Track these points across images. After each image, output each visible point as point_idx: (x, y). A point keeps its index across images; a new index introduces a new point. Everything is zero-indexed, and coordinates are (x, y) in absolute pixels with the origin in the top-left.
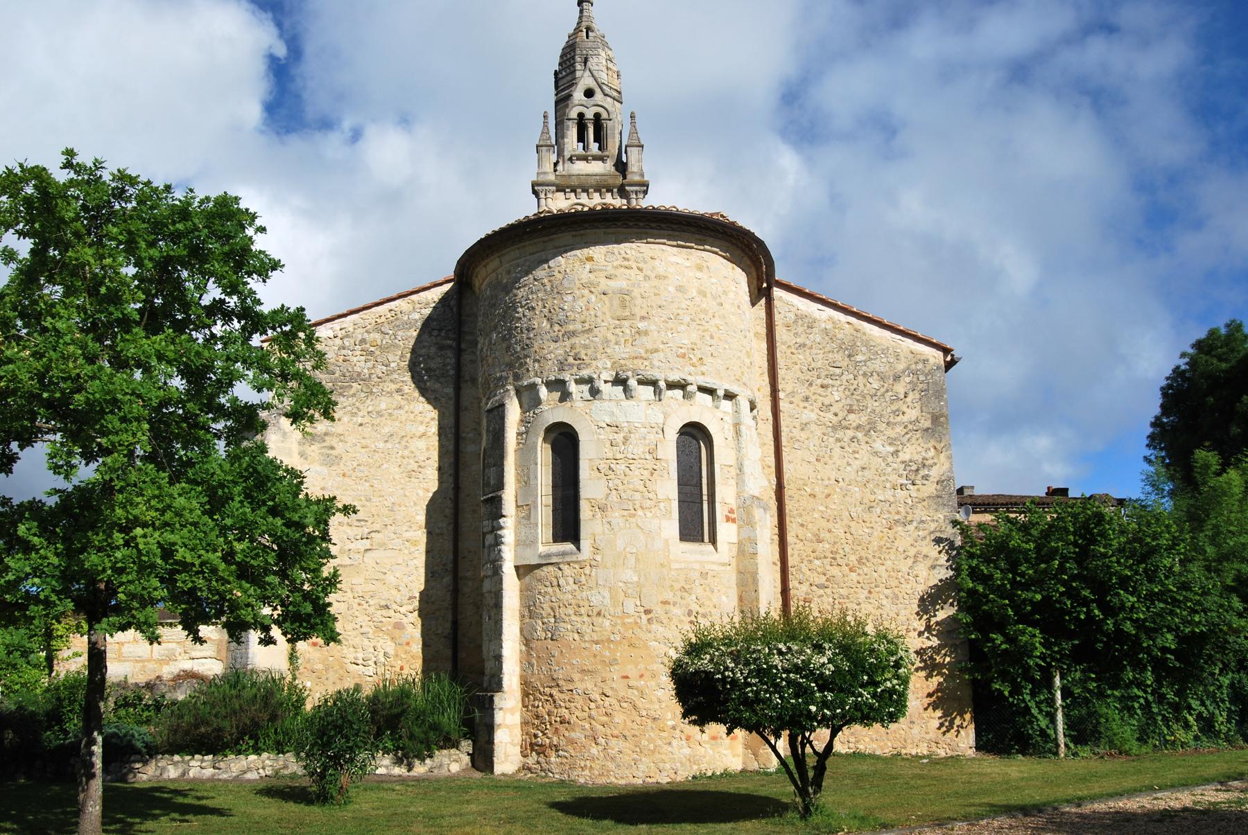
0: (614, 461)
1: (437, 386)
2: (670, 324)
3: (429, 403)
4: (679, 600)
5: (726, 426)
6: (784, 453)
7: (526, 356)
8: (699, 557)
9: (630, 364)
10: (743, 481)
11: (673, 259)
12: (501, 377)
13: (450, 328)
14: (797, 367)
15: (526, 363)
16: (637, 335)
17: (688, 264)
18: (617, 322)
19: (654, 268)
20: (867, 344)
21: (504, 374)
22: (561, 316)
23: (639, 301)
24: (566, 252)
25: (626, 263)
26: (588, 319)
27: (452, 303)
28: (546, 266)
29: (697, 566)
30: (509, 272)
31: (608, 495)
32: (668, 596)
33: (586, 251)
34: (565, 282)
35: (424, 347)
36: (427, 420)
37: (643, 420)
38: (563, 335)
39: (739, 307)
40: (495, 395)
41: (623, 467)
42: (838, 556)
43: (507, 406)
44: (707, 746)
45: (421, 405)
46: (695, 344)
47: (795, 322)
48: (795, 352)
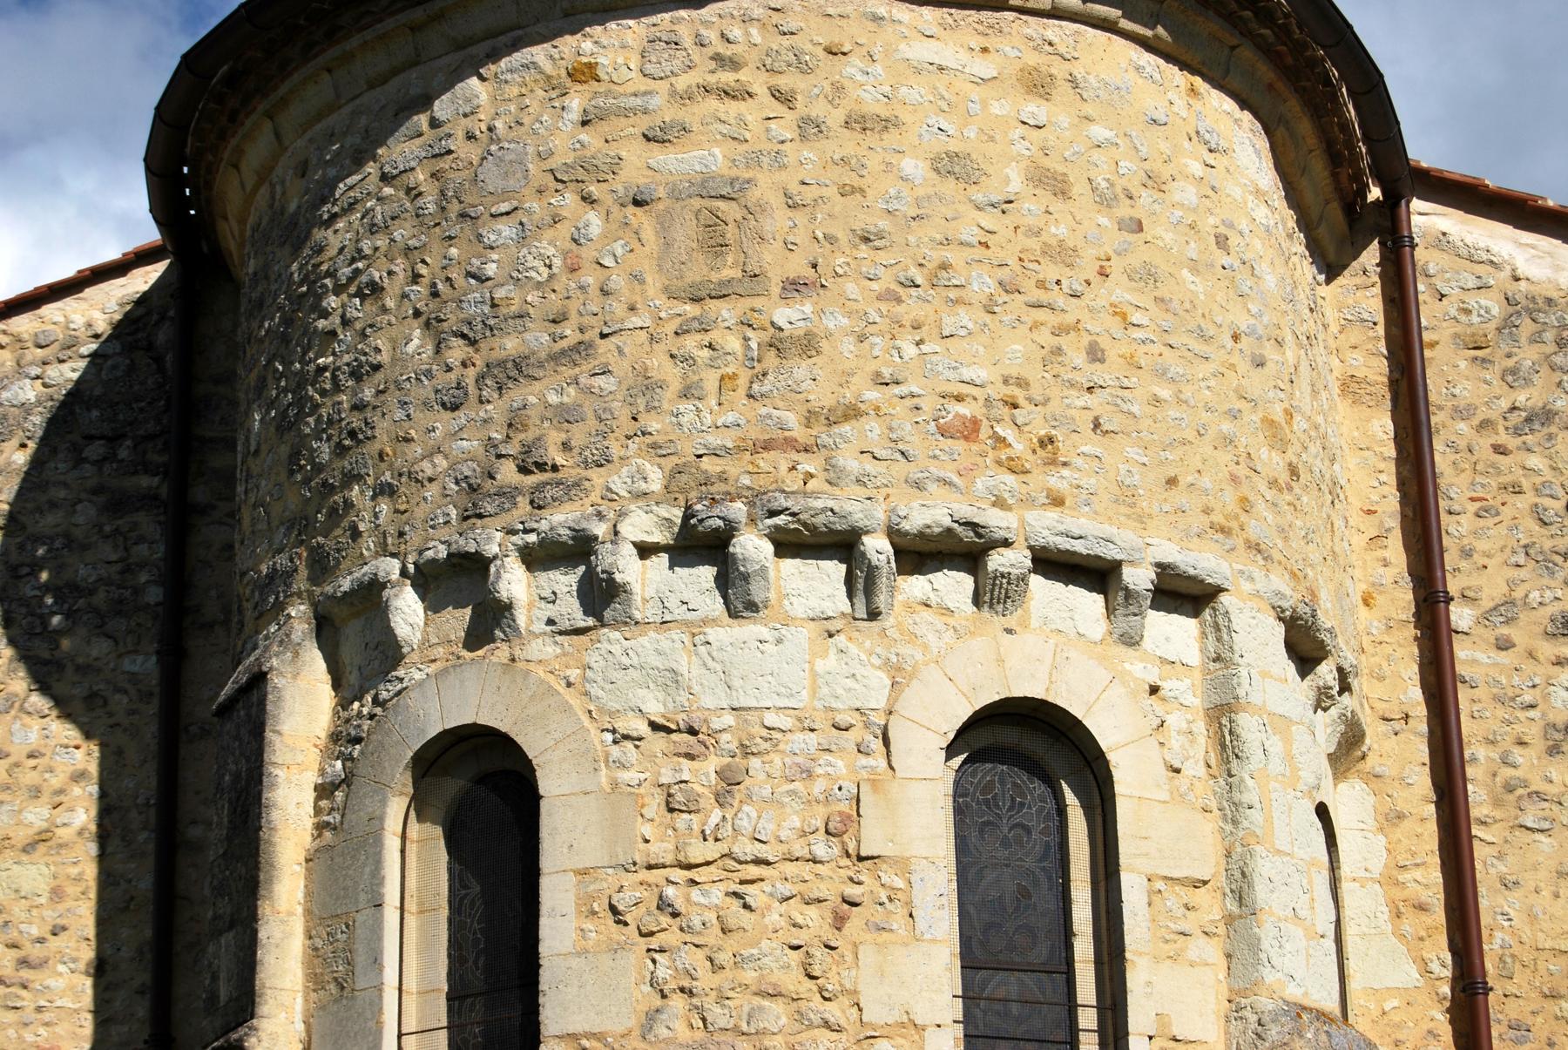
0: (679, 875)
1: (100, 649)
2: (911, 308)
3: (67, 714)
5: (1175, 720)
6: (1480, 851)
7: (351, 478)
9: (739, 472)
10: (1255, 946)
11: (922, 51)
12: (273, 575)
13: (151, 427)
14: (1523, 503)
15: (348, 505)
16: (771, 359)
17: (984, 67)
18: (690, 309)
19: (838, 88)
21: (282, 561)
22: (474, 303)
23: (778, 221)
24: (494, 56)
25: (727, 78)
26: (574, 306)
27: (163, 336)
28: (422, 120)
30: (303, 170)
31: (652, 1016)
33: (568, 43)
34: (491, 176)
35: (53, 505)
36: (55, 782)
37: (803, 700)
38: (480, 379)
39: (1222, 242)
40: (255, 648)
41: (717, 895)
43: (276, 680)
45: (36, 724)
46: (1022, 383)
47: (1507, 326)
48: (1512, 442)
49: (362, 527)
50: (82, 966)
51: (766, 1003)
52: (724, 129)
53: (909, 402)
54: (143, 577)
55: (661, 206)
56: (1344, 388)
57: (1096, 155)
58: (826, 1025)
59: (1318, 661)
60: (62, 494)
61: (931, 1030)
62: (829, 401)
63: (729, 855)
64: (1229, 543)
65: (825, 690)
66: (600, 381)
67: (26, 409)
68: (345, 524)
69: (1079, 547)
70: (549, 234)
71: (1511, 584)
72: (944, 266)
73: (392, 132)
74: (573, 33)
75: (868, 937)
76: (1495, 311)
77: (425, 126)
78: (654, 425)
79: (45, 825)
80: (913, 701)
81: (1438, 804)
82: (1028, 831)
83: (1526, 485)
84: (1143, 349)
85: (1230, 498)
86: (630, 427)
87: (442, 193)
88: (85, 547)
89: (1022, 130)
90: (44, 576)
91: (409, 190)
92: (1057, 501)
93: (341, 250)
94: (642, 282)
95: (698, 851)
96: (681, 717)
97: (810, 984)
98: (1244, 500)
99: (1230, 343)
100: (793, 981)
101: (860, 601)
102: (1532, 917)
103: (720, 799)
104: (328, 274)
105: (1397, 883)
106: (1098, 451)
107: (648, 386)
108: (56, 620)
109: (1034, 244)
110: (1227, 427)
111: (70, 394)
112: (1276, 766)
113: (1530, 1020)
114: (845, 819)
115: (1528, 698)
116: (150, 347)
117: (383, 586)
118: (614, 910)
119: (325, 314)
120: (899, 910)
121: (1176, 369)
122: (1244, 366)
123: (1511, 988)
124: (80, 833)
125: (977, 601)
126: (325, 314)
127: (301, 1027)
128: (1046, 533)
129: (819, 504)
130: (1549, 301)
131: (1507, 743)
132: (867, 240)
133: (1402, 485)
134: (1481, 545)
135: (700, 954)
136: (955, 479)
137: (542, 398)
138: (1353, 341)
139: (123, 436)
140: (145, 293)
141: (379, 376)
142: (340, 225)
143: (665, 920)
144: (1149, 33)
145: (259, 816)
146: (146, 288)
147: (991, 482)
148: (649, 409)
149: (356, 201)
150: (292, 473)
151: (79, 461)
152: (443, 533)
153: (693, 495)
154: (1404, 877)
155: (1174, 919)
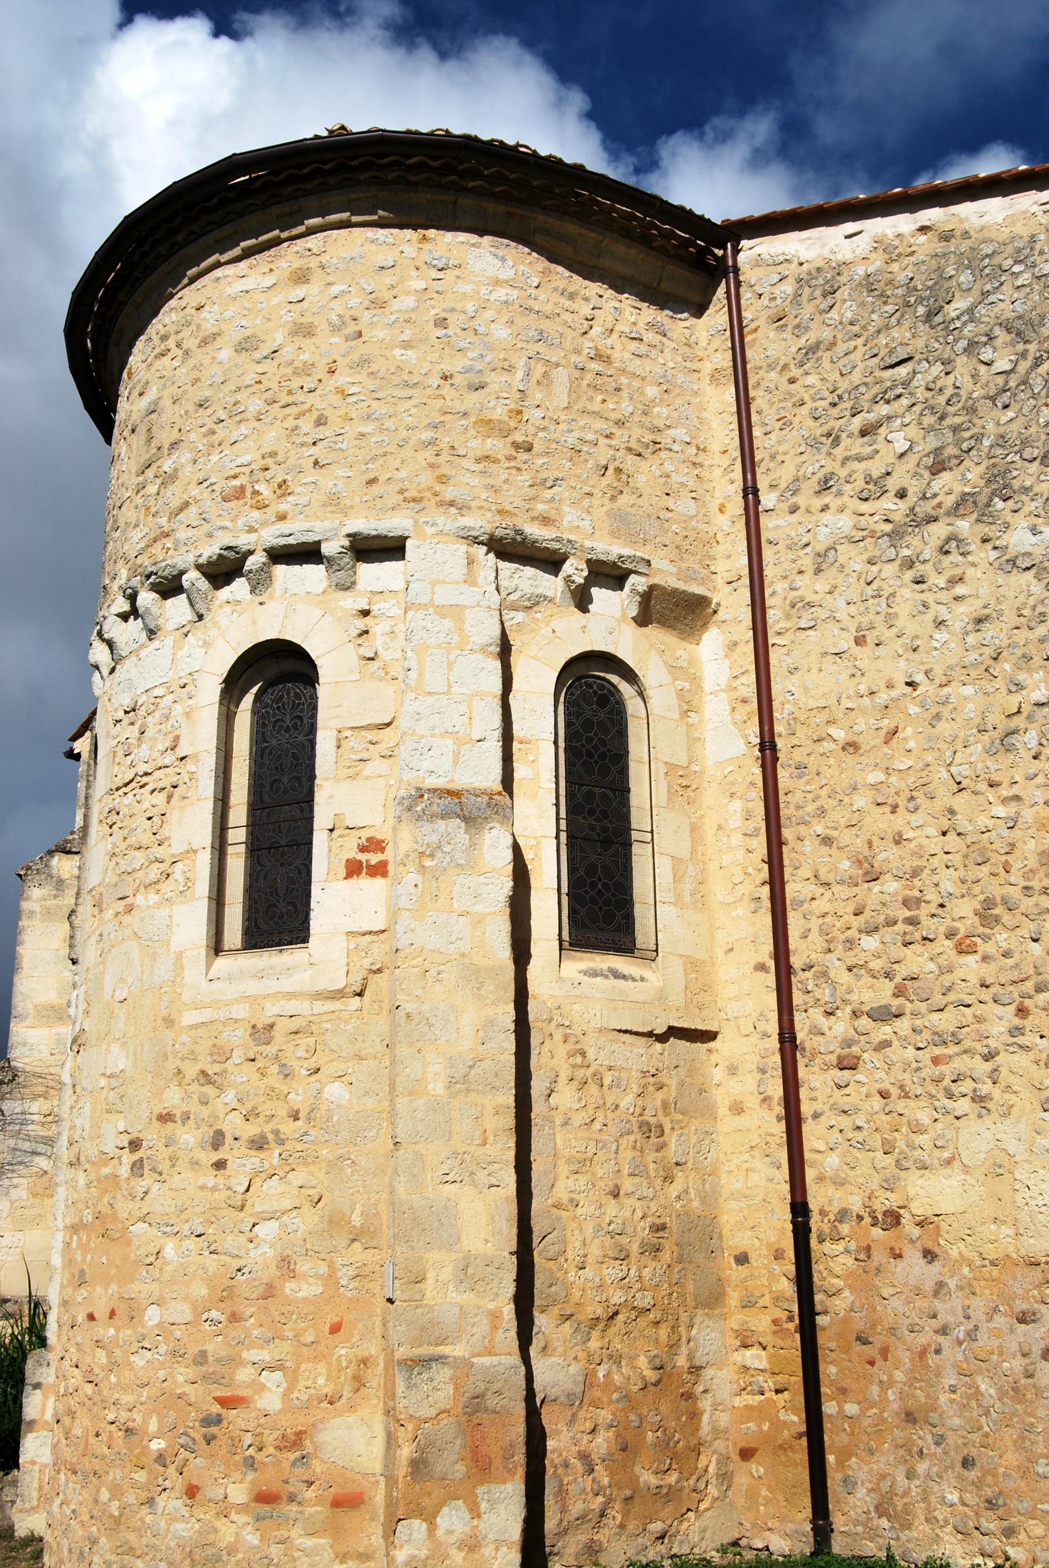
2: (221, 432)
4: (194, 1107)
8: (253, 987)
14: (804, 411)
20: (972, 261)
29: (241, 1011)
32: (173, 1098)
42: (923, 912)
44: (241, 1519)
69: (291, 541)
128: (270, 539)
132: (201, 405)
144: (375, 217)
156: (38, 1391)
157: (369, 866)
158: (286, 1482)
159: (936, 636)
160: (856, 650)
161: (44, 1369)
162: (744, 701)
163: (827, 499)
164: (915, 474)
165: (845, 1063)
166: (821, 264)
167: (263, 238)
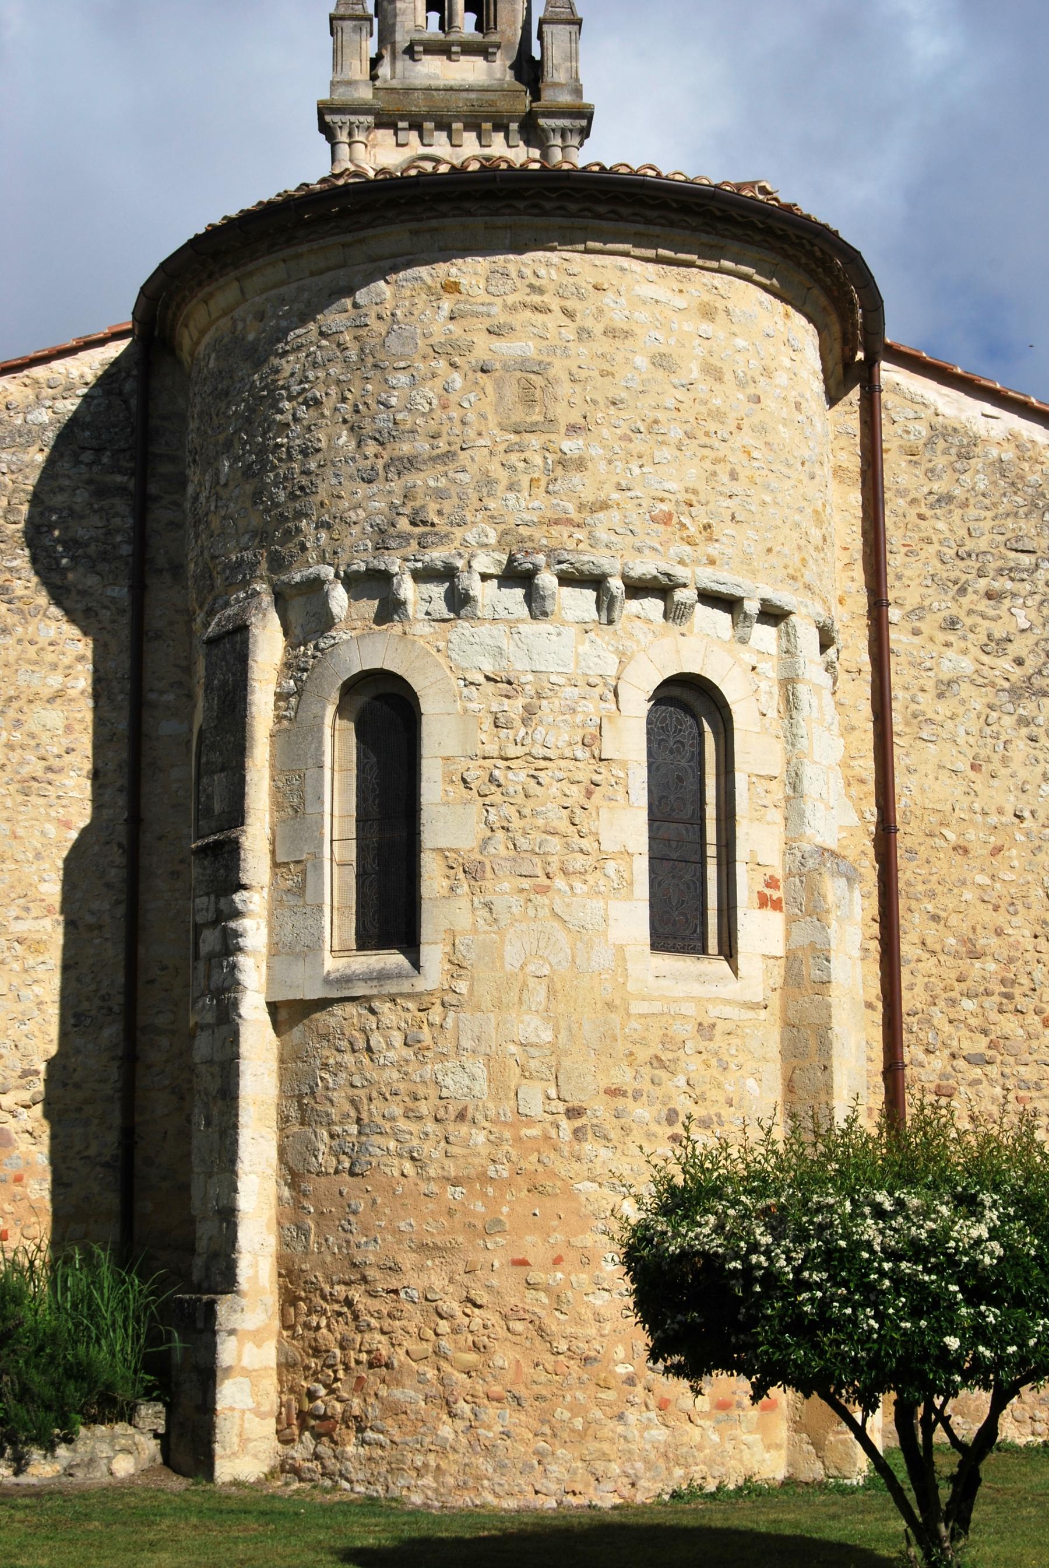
2: (638, 445)
3: (72, 619)
4: (646, 1086)
5: (764, 686)
6: (897, 751)
7: (300, 515)
9: (542, 540)
10: (801, 814)
11: (647, 291)
12: (240, 563)
13: (123, 445)
14: (932, 549)
15: (299, 530)
16: (559, 471)
17: (680, 302)
18: (513, 438)
19: (601, 311)
21: (248, 555)
23: (565, 389)
24: (395, 269)
25: (536, 299)
26: (445, 429)
27: (129, 386)
28: (348, 302)
31: (486, 842)
32: (624, 1077)
33: (442, 268)
35: (62, 489)
36: (66, 661)
37: (571, 669)
38: (386, 467)
39: (798, 406)
41: (522, 776)
42: (1017, 991)
43: (254, 630)
44: (707, 1423)
45: (54, 625)
46: (695, 492)
47: (930, 443)
48: (928, 513)
49: (308, 545)
50: (84, 773)
51: (549, 837)
52: (535, 331)
53: (636, 501)
54: (119, 539)
55: (497, 374)
56: (835, 473)
57: (738, 356)
58: (581, 851)
59: (828, 647)
60: (67, 482)
61: (636, 856)
62: (591, 498)
63: (529, 754)
64: (797, 585)
65: (583, 664)
66: (460, 476)
67: (43, 427)
68: (296, 541)
69: (723, 589)
70: (430, 384)
71: (923, 597)
72: (656, 422)
73: (327, 306)
74: (445, 262)
75: (605, 803)
76: (924, 433)
77: (350, 307)
78: (492, 505)
79: (60, 687)
80: (632, 673)
81: (874, 723)
82: (683, 744)
83: (935, 539)
84: (758, 472)
85: (797, 558)
86: (478, 505)
87: (362, 350)
88: (82, 517)
89: (698, 340)
90: (57, 533)
91: (339, 345)
92: (712, 562)
93: (292, 374)
94: (486, 419)
95: (512, 751)
96: (503, 674)
97: (573, 828)
98: (804, 560)
99: (800, 467)
100: (564, 826)
101: (604, 614)
102: (923, 790)
103: (525, 722)
104: (283, 387)
105: (849, 766)
106: (733, 533)
107: (488, 482)
108: (64, 561)
109: (703, 409)
110: (797, 517)
111: (70, 420)
112: (815, 714)
113: (917, 848)
114: (593, 737)
115: (928, 664)
116: (120, 393)
117: (324, 582)
118: (464, 781)
119: (281, 412)
120: (620, 789)
121: (774, 485)
122: (805, 480)
123: (908, 830)
124: (82, 693)
125: (666, 616)
126: (281, 412)
127: (268, 831)
129: (586, 558)
130: (955, 430)
131: (915, 690)
132: (614, 404)
133: (864, 534)
134: (907, 573)
135: (513, 808)
136: (659, 547)
137: (425, 482)
138: (842, 445)
139: (105, 449)
140: (117, 359)
141: (320, 456)
142: (291, 358)
143: (494, 788)
144: (768, 282)
145: (245, 709)
146: (117, 355)
147: (678, 550)
148: (489, 495)
149: (302, 345)
150: (256, 503)
151: (77, 462)
152: (364, 556)
153: (515, 548)
154: (853, 763)
155: (760, 798)
156: (233, 1338)
157: (772, 901)
158: (734, 1393)
159: (1044, 787)
160: (972, 775)
161: (238, 1315)
162: (862, 781)
163: (951, 638)
164: (1032, 651)
165: (944, 1091)
166: (958, 426)
167: (682, 256)
